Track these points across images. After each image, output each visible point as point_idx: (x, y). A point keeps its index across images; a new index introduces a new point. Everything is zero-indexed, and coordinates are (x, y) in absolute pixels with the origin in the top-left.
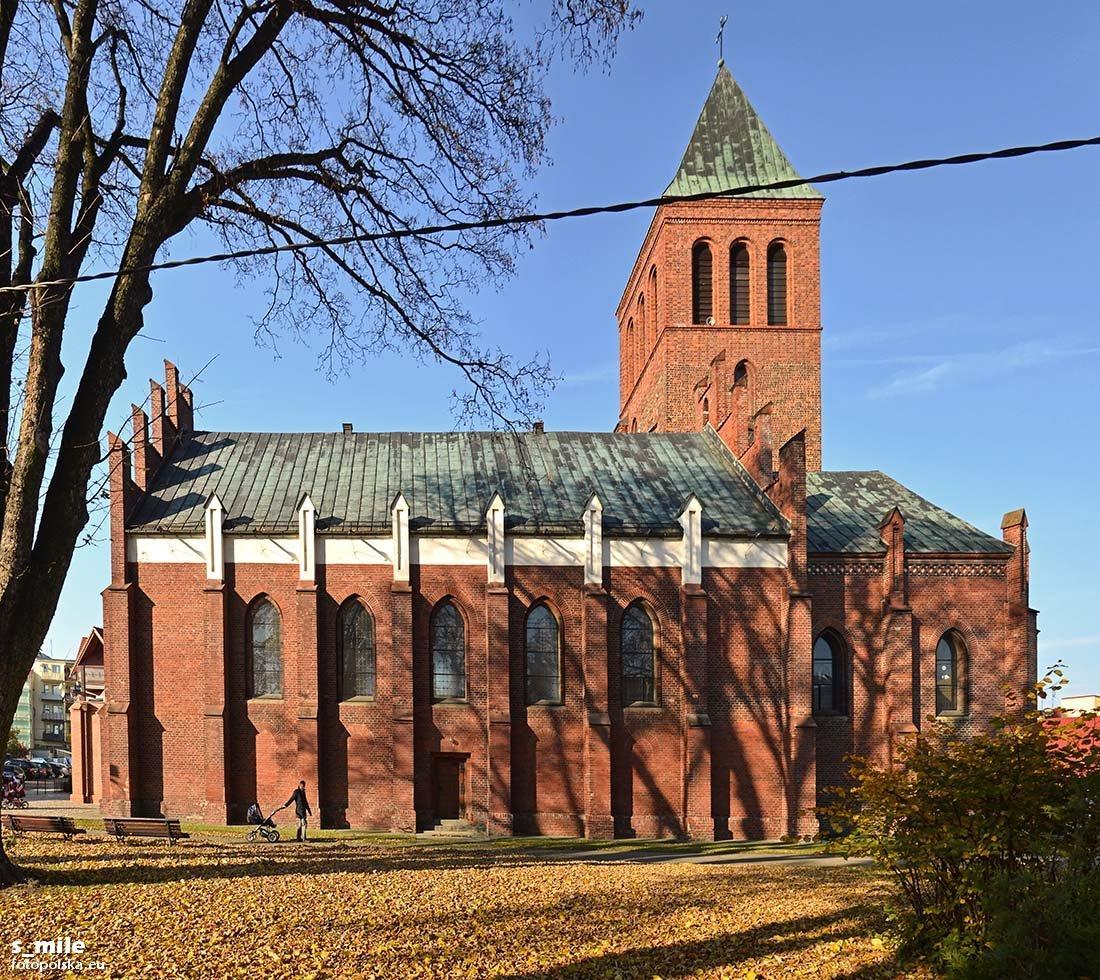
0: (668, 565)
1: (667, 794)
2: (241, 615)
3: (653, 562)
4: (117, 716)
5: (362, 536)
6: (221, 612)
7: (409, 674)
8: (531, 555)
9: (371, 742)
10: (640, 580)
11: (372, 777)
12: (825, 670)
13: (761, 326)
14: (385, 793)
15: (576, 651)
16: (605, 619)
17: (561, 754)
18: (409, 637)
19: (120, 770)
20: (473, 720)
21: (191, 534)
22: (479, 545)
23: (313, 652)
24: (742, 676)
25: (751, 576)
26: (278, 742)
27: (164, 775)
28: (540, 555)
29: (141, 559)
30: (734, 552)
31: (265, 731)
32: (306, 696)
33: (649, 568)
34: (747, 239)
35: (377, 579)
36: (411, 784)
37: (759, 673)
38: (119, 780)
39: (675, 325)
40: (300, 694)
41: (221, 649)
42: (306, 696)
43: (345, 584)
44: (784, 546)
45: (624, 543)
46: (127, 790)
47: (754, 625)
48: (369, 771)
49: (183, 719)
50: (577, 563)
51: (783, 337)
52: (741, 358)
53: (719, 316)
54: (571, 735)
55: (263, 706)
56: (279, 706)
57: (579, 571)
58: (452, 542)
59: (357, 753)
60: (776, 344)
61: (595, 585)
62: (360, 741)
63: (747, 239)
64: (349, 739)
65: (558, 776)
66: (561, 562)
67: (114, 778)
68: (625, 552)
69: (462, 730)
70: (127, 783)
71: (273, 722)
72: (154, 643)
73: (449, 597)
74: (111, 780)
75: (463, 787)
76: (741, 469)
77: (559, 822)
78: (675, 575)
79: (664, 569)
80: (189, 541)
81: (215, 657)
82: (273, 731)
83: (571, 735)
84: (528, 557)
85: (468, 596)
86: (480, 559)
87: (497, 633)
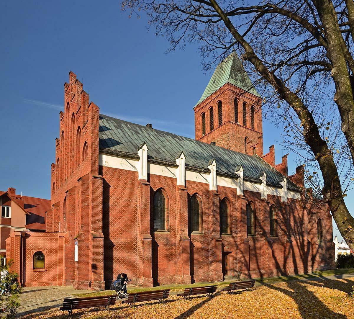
0: (278, 196)
1: (279, 262)
2: (156, 198)
3: (275, 194)
4: (98, 239)
5: (200, 172)
6: (149, 194)
7: (218, 224)
8: (248, 187)
9: (201, 249)
10: (273, 199)
11: (202, 262)
12: (194, 218)
13: (250, 128)
14: (206, 268)
15: (259, 218)
16: (269, 209)
17: (255, 251)
18: (218, 210)
19: (98, 266)
20: (232, 240)
21: (131, 158)
22: (234, 181)
23: (186, 214)
24: (293, 228)
25: (293, 201)
26: (167, 250)
27: (114, 267)
28: (250, 188)
29: (104, 164)
30: (290, 194)
31: (162, 245)
32: (183, 231)
33: (274, 195)
34: (247, 103)
35: (204, 188)
36: (221, 263)
37: (296, 228)
38: (97, 271)
39: (231, 121)
40: (181, 230)
41: (148, 210)
42: (183, 231)
43: (193, 189)
44: (299, 194)
45: (269, 188)
46: (102, 276)
47: (295, 214)
48: (201, 260)
49: (125, 240)
50: (259, 192)
51: (255, 133)
52: (246, 136)
53: (240, 122)
54: (258, 245)
55: (161, 235)
56: (168, 235)
57: (259, 194)
58: (226, 179)
59: (197, 253)
60: (253, 134)
61: (265, 199)
62: (198, 248)
63: (247, 103)
64: (194, 248)
65: (255, 259)
66: (255, 191)
67: (95, 270)
68: (269, 190)
69: (229, 244)
70: (103, 272)
71: (165, 242)
72: (110, 204)
73: (226, 197)
74: (93, 271)
75: (227, 264)
76: (275, 170)
77: (256, 274)
78: (280, 199)
79: (277, 196)
80: (130, 161)
81: (146, 213)
82: (165, 245)
83: (258, 245)
84: (247, 187)
85: (231, 198)
86: (233, 186)
87: (242, 212)
